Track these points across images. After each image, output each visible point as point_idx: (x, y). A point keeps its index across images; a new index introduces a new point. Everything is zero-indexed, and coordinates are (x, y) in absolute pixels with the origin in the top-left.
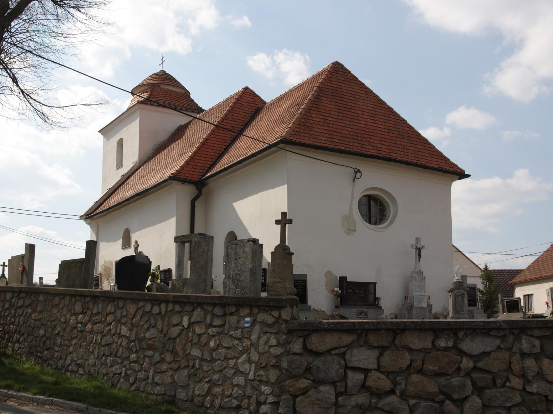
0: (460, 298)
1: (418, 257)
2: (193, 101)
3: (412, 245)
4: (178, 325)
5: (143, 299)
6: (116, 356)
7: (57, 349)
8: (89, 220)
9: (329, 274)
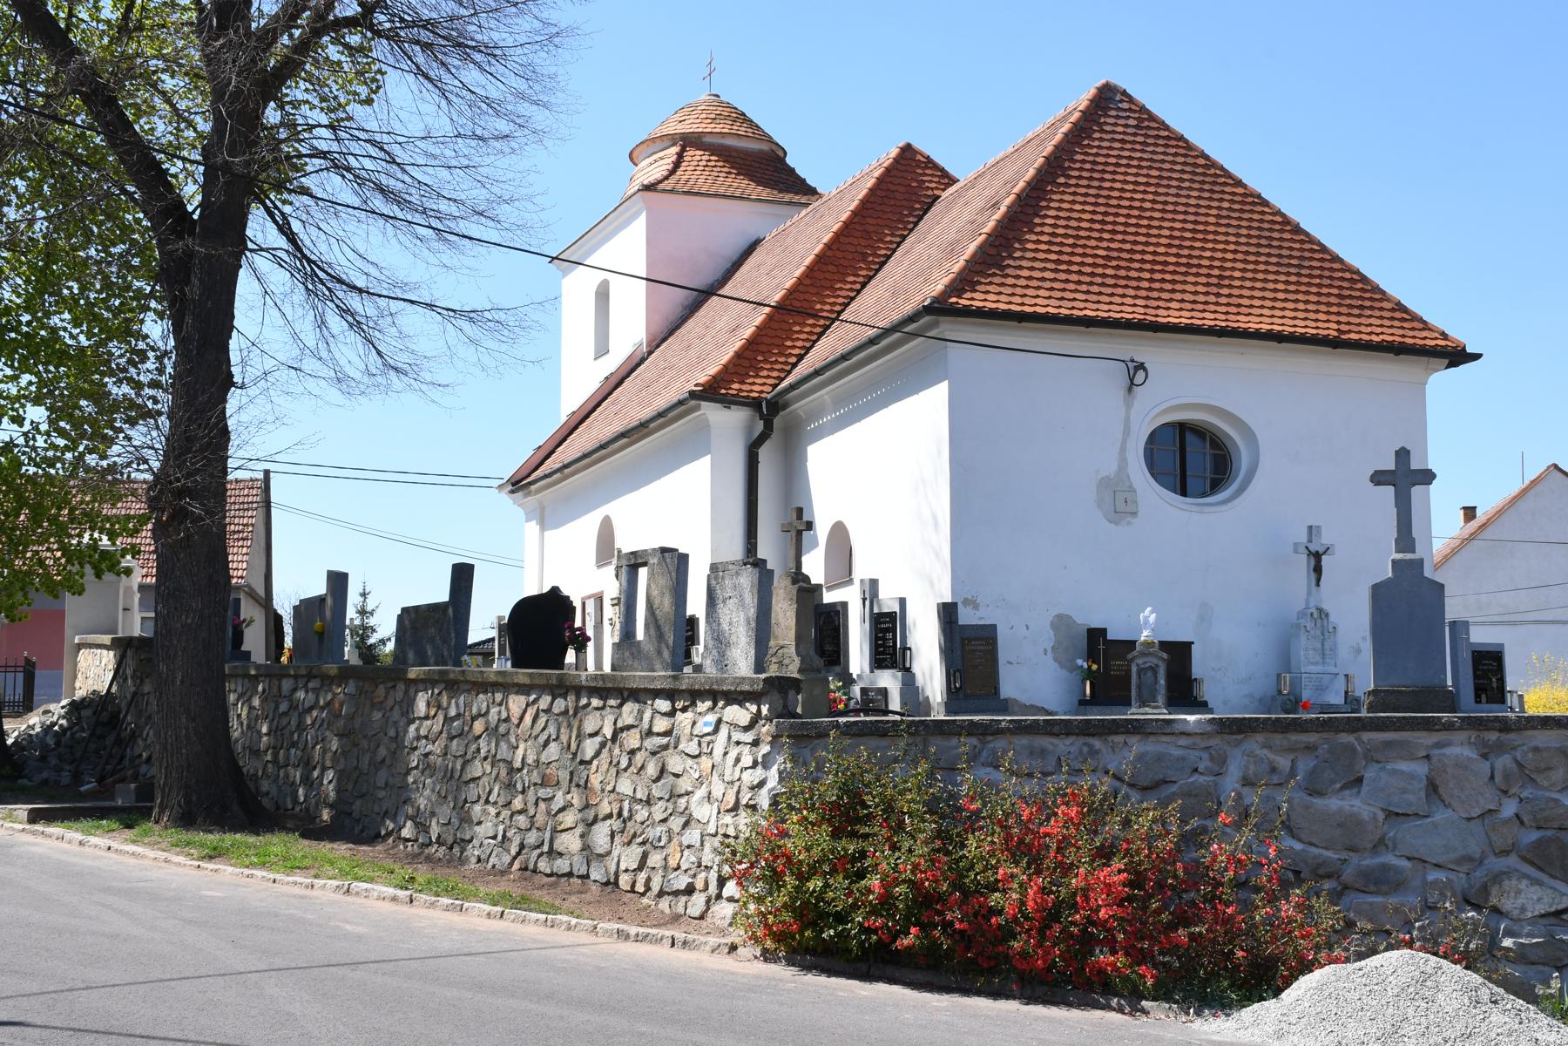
0: (1150, 674)
1: (1313, 576)
3: (1296, 544)
4: (596, 734)
6: (487, 802)
7: (381, 794)
8: (519, 495)
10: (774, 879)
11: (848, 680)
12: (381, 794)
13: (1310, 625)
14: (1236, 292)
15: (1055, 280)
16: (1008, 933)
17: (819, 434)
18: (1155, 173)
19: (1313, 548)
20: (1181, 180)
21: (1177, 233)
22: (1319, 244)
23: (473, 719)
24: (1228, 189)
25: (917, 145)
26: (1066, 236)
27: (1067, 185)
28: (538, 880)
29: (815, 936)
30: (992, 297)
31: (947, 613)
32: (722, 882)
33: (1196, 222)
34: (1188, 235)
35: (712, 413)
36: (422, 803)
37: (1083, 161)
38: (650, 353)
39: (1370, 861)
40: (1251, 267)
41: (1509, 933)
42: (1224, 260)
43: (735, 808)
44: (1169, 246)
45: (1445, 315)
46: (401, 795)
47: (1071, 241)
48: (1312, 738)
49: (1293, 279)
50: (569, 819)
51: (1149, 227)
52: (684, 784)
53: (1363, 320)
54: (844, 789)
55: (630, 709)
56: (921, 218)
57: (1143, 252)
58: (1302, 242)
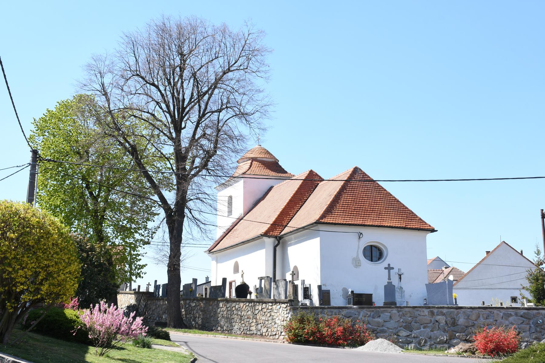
9: (345, 290)
10: (290, 331)
25: (314, 170)
28: (248, 334)
29: (298, 339)
31: (320, 287)
32: (281, 333)
35: (266, 239)
36: (222, 323)
38: (244, 217)
39: (381, 328)
45: (430, 221)
46: (217, 322)
48: (373, 309)
50: (253, 324)
52: (274, 317)
54: (301, 317)
56: (314, 189)
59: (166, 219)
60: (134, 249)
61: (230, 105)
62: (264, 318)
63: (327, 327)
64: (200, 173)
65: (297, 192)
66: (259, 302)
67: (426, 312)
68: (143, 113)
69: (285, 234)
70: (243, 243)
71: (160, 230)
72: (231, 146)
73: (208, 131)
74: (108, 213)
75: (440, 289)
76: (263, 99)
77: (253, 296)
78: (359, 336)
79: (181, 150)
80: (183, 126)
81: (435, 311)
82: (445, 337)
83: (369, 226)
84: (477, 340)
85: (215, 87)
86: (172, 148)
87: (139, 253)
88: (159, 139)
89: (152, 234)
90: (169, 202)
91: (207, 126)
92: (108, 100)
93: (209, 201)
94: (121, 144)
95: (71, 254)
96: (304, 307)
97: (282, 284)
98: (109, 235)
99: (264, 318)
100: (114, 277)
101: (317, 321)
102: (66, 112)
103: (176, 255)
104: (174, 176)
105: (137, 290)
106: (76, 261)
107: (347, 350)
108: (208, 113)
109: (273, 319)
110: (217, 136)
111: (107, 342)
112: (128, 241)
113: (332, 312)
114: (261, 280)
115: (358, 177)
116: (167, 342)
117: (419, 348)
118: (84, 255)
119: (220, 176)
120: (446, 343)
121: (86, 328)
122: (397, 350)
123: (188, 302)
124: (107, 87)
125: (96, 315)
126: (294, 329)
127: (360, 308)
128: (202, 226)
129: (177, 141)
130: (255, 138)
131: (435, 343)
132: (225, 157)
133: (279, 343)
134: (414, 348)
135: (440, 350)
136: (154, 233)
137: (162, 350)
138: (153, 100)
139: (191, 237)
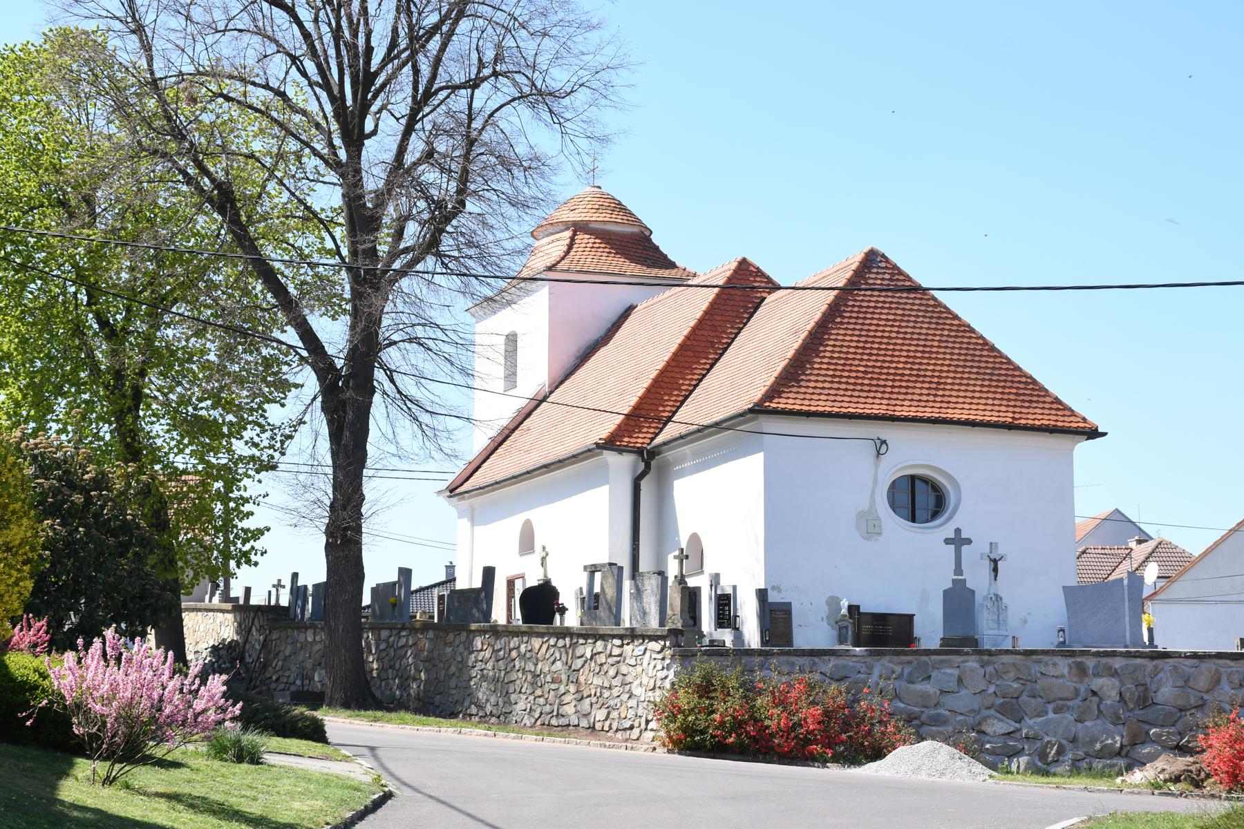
2: (657, 248)
5: (551, 635)
7: (453, 692)
9: (834, 602)
11: (702, 635)
12: (453, 692)
13: (990, 605)
14: (947, 393)
15: (831, 388)
16: (772, 735)
17: (682, 474)
18: (900, 312)
19: (992, 557)
20: (917, 316)
21: (912, 354)
22: (1007, 358)
23: (511, 650)
24: (948, 322)
25: (751, 259)
26: (839, 358)
27: (842, 323)
28: (552, 724)
29: (693, 741)
30: (791, 401)
31: (762, 595)
32: (647, 722)
33: (925, 346)
34: (919, 355)
35: (610, 457)
37: (853, 306)
38: (551, 392)
39: (933, 712)
40: (959, 375)
41: (989, 742)
42: (941, 371)
43: (654, 688)
44: (906, 363)
46: (468, 693)
47: (842, 362)
48: (910, 658)
49: (987, 383)
50: (567, 698)
51: (894, 350)
52: (629, 679)
53: (1031, 411)
54: (704, 677)
55: (600, 644)
56: (752, 315)
57: (889, 368)
58: (995, 357)
59: (320, 399)
60: (231, 483)
61: (504, 68)
62: (597, 681)
63: (777, 706)
64: (419, 267)
65: (701, 321)
66: (586, 636)
67: (1063, 666)
68: (250, 87)
69: (665, 444)
70: (547, 467)
71: (303, 429)
72: (506, 188)
73: (442, 146)
74: (154, 382)
75: (1106, 597)
76: (600, 48)
77: (572, 619)
78: (870, 733)
79: (361, 197)
80: (369, 125)
81: (1090, 663)
82: (1118, 738)
83: (906, 419)
84: (1210, 746)
85: (461, 15)
86: (339, 191)
87: (246, 495)
88: (301, 166)
89: (282, 442)
90: (330, 350)
91: (437, 130)
92: (147, 48)
93: (447, 348)
94: (189, 180)
95: (10, 495)
96: (717, 650)
97: (650, 585)
98: (159, 442)
99: (597, 681)
100: (173, 562)
101: (750, 691)
102: (21, 81)
103: (349, 500)
104: (344, 274)
105: (241, 602)
106: (26, 514)
107: (835, 771)
108: (441, 89)
109: (623, 684)
110: (466, 156)
111: (130, 744)
112: (214, 460)
113: (793, 664)
114: (592, 573)
115: (874, 279)
116: (317, 748)
117: (1043, 767)
118: (78, 498)
119: (476, 277)
120: (1119, 754)
121: (65, 707)
122: (975, 775)
123: (384, 634)
124: (142, 10)
125: (92, 668)
126: (683, 712)
127: (871, 653)
128: (425, 418)
129: (350, 173)
130: (576, 164)
131: (1087, 754)
132: (491, 221)
133: (641, 752)
134: (1026, 769)
135: (1101, 775)
136: (291, 437)
137: (291, 768)
138: (281, 49)
139: (393, 449)
